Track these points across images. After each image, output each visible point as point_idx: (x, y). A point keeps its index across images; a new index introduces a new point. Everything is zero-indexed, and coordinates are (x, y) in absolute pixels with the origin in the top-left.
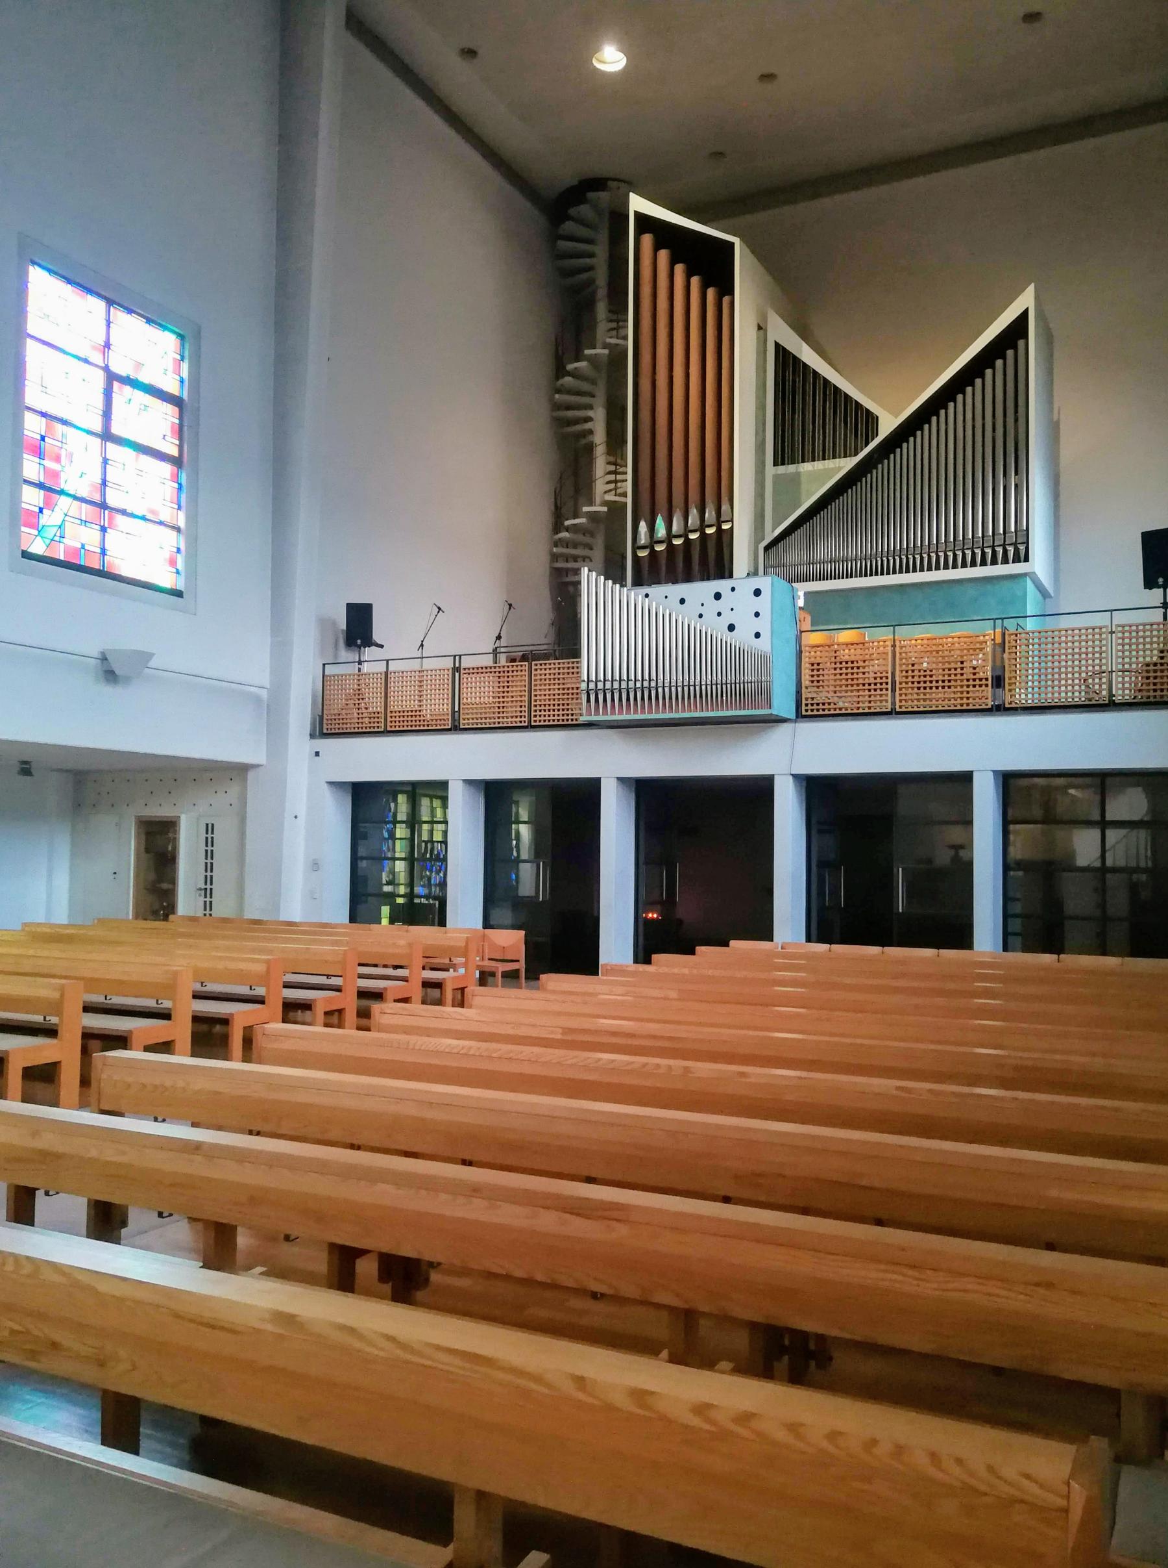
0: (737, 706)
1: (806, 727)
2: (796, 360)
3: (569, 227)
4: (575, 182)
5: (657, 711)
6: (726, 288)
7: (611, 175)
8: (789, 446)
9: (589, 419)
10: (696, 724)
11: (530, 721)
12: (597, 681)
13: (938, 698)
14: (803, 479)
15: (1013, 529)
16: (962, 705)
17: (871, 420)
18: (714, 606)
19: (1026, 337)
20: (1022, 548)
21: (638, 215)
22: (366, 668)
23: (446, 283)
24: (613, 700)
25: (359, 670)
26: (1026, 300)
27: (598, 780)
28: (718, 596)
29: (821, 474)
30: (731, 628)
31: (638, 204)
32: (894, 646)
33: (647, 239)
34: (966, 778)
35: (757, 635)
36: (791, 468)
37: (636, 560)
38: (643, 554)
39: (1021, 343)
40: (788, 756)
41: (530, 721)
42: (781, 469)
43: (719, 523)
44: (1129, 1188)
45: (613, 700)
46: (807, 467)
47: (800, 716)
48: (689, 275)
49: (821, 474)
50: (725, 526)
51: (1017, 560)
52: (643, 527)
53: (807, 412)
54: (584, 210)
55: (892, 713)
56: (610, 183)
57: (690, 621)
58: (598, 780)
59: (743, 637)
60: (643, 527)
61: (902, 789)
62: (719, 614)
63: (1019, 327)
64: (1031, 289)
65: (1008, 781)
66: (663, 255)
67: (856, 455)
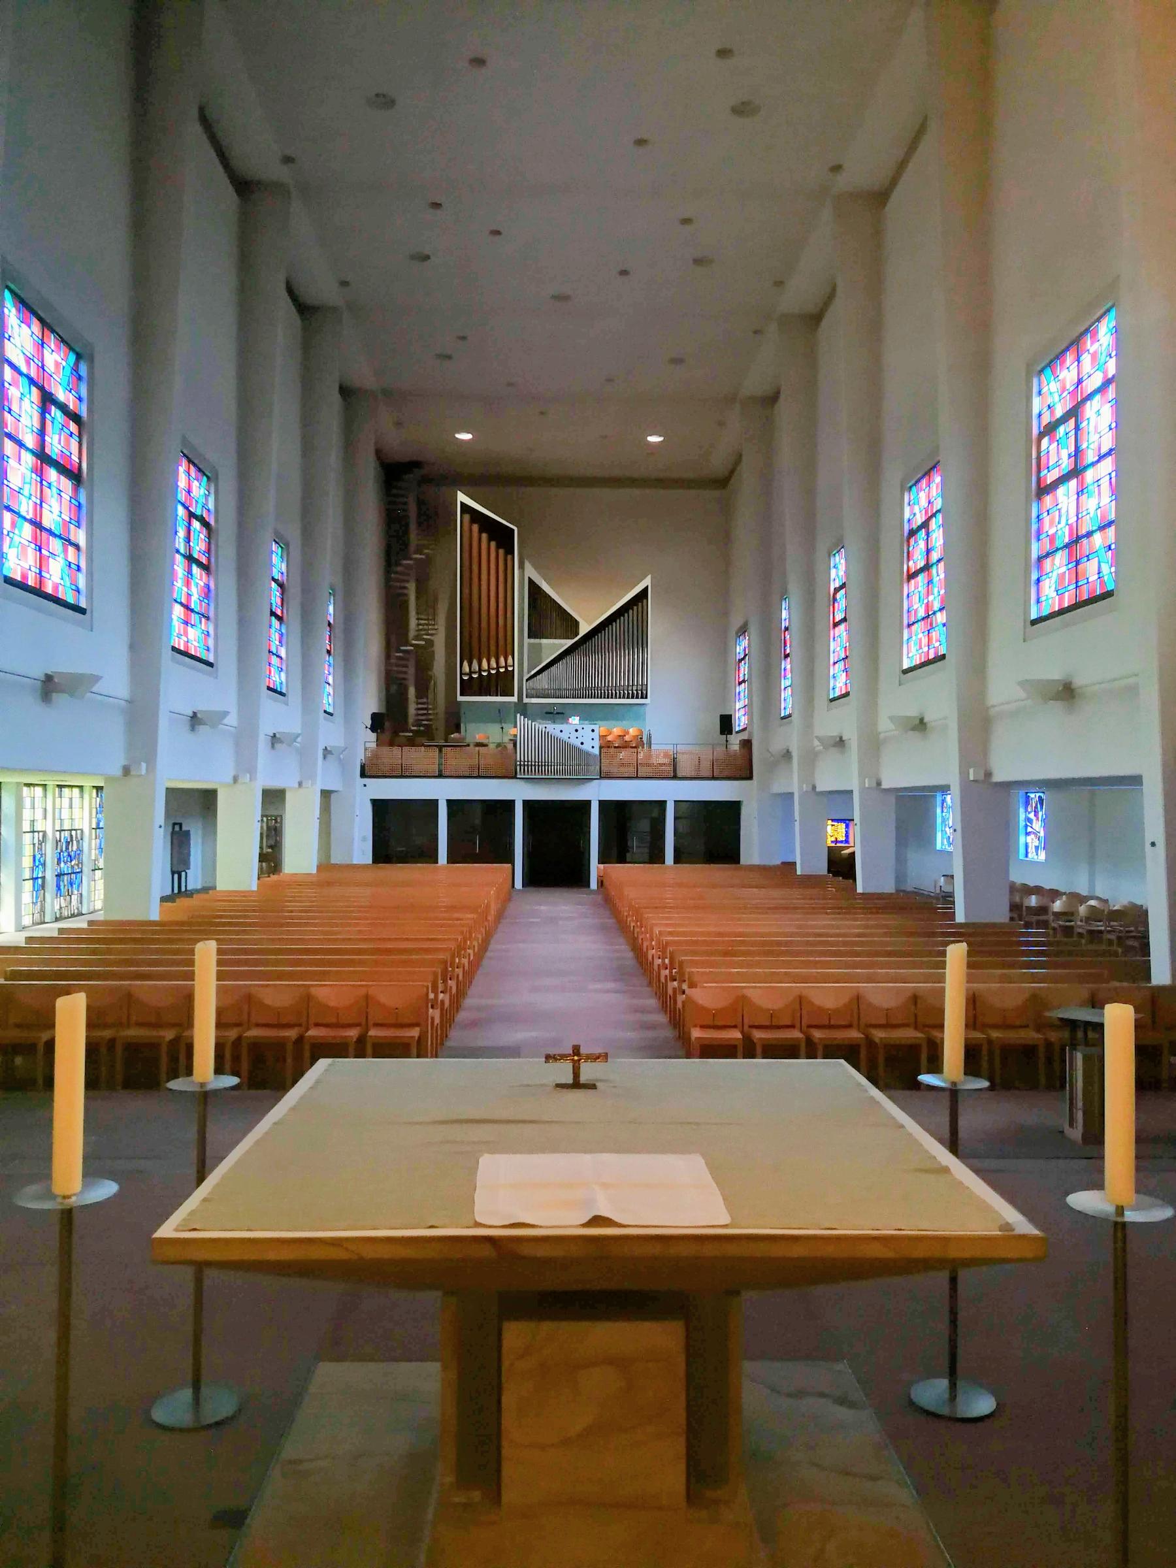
1: (605, 782)
2: (539, 588)
9: (405, 588)
17: (575, 624)
23: (72, 358)
26: (647, 582)
27: (590, 801)
29: (554, 646)
31: (462, 497)
33: (467, 517)
34: (665, 802)
36: (537, 641)
37: (461, 679)
40: (596, 792)
42: (532, 641)
43: (506, 667)
44: (776, 908)
46: (544, 641)
47: (601, 778)
48: (490, 540)
50: (510, 669)
52: (466, 664)
53: (546, 616)
58: (590, 801)
59: (587, 747)
60: (466, 664)
63: (644, 593)
64: (649, 577)
65: (450, 803)
66: (475, 527)
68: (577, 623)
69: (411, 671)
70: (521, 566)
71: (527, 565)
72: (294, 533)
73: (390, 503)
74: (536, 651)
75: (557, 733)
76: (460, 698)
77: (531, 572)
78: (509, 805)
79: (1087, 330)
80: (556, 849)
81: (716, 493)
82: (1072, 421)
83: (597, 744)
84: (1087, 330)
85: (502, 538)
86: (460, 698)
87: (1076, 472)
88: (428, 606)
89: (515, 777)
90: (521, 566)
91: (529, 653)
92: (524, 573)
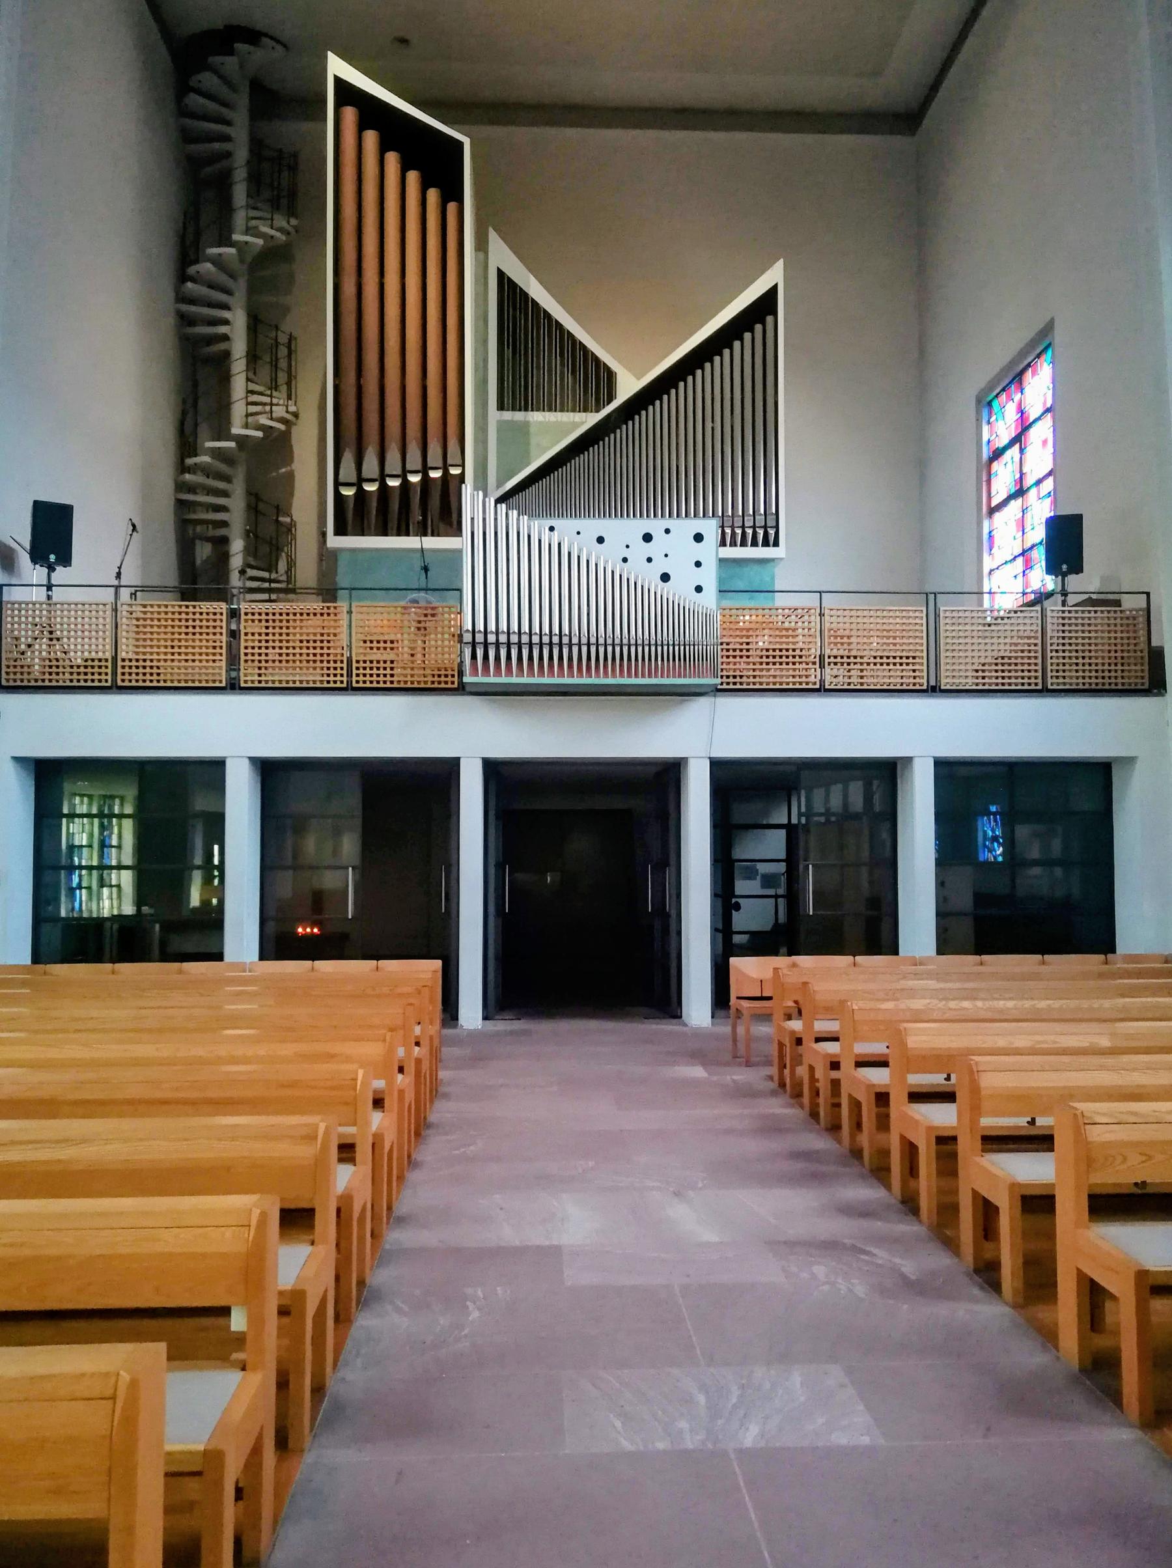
0: (661, 669)
2: (525, 295)
3: (207, 80)
4: (219, 24)
5: (598, 675)
6: (452, 192)
7: (265, 30)
8: (517, 392)
10: (565, 694)
11: (114, 680)
12: (520, 633)
13: (879, 677)
14: (532, 430)
15: (762, 511)
16: (1077, 684)
18: (641, 550)
19: (775, 314)
20: (772, 532)
21: (338, 80)
22: (57, 594)
24: (531, 658)
25: (49, 597)
26: (773, 276)
28: (648, 538)
29: (555, 428)
30: (665, 577)
31: (337, 67)
32: (821, 615)
33: (350, 113)
35: (699, 589)
36: (519, 416)
37: (338, 496)
38: (348, 492)
39: (770, 319)
40: (699, 736)
41: (114, 680)
42: (508, 415)
45: (531, 658)
46: (536, 417)
49: (555, 428)
50: (455, 471)
51: (766, 543)
53: (536, 356)
54: (229, 64)
55: (821, 690)
56: (265, 40)
57: (614, 566)
58: (459, 759)
59: (680, 590)
60: (348, 458)
61: (805, 774)
62: (649, 560)
63: (766, 305)
64: (780, 264)
66: (371, 138)
67: (597, 411)
68: (611, 375)
69: (237, 504)
70: (482, 245)
71: (495, 241)
72: (354, 447)
73: (187, 137)
74: (516, 437)
75: (585, 547)
76: (334, 541)
77: (502, 256)
78: (441, 776)
79: (1029, 365)
80: (580, 903)
81: (898, 142)
82: (1017, 446)
83: (709, 577)
84: (1029, 365)
85: (436, 163)
86: (334, 541)
87: (1020, 492)
88: (274, 357)
89: (462, 689)
90: (482, 245)
91: (497, 441)
92: (489, 259)
